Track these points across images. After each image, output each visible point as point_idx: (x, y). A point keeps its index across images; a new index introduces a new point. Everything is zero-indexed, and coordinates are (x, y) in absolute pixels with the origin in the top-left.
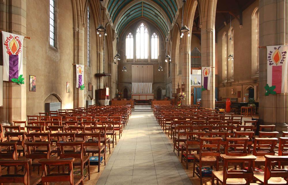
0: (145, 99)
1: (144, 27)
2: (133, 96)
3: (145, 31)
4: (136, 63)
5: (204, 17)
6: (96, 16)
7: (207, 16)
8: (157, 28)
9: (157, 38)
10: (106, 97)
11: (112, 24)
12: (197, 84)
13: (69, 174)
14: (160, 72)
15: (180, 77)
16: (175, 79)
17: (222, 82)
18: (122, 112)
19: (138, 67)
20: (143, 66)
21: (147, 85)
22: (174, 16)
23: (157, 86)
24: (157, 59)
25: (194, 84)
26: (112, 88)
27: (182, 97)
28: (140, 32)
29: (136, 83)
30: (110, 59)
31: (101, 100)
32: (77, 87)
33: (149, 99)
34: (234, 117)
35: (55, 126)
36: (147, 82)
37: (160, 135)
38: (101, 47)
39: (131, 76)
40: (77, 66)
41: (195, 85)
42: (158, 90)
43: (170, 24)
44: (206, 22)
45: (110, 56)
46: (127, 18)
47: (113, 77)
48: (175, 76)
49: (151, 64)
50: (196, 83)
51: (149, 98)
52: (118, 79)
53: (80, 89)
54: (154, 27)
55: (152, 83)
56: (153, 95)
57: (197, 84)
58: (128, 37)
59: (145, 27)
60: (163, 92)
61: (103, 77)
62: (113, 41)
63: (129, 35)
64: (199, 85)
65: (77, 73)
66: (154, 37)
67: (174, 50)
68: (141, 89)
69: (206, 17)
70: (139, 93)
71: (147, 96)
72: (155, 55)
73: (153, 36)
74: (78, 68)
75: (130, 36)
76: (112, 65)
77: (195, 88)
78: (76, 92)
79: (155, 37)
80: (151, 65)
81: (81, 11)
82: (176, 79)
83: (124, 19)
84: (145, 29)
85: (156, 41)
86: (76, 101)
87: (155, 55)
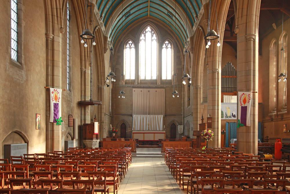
0: (152, 139)
1: (152, 32)
3: (153, 38)
4: (139, 85)
5: (242, 17)
9: (171, 48)
10: (94, 136)
12: (230, 117)
15: (204, 106)
16: (197, 109)
17: (269, 114)
19: (141, 91)
20: (149, 89)
22: (197, 16)
23: (170, 119)
24: (171, 80)
25: (227, 117)
27: (207, 137)
28: (145, 40)
29: (139, 116)
30: (100, 80)
31: (87, 141)
32: (52, 120)
38: (87, 62)
39: (132, 105)
40: (52, 90)
41: (227, 119)
48: (197, 105)
50: (229, 115)
51: (158, 137)
54: (165, 33)
55: (162, 116)
57: (230, 117)
58: (127, 46)
59: (153, 32)
60: (180, 129)
61: (90, 106)
62: (105, 53)
63: (129, 44)
64: (233, 118)
65: (51, 101)
66: (167, 48)
70: (144, 131)
71: (145, 134)
72: (168, 74)
73: (164, 46)
74: (53, 93)
75: (130, 46)
77: (228, 122)
78: (50, 129)
79: (168, 47)
80: (162, 89)
84: (152, 36)
86: (50, 141)
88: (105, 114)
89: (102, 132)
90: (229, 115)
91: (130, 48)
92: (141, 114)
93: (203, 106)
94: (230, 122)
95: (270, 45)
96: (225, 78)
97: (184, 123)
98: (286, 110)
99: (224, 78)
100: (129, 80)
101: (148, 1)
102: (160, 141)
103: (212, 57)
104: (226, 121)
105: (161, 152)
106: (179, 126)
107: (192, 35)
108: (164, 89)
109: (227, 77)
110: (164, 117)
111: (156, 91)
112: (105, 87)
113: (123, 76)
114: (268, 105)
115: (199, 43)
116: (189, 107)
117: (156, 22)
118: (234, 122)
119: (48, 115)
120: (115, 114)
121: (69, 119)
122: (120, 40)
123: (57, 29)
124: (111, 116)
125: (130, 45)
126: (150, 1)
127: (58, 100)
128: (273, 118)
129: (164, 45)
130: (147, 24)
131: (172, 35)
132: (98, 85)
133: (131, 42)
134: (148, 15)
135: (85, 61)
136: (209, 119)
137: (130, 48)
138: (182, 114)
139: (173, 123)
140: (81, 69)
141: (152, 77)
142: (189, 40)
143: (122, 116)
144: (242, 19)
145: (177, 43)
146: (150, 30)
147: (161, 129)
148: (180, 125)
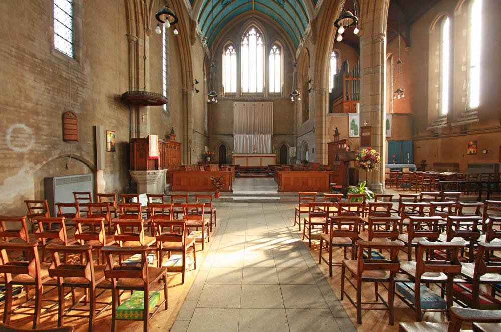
0: (258, 165)
1: (256, 34)
2: (236, 159)
3: (258, 42)
4: (242, 98)
5: (367, 13)
7: (374, 11)
8: (282, 34)
9: (280, 54)
10: (149, 163)
13: (182, 235)
14: (283, 115)
15: (332, 118)
16: (321, 122)
17: (427, 129)
22: (302, 37)
23: (280, 139)
24: (280, 93)
26: (191, 142)
27: (369, 163)
28: (248, 45)
29: (242, 136)
31: (135, 172)
33: (266, 165)
34: (464, 208)
36: (262, 134)
37: (276, 207)
39: (233, 123)
42: (282, 147)
43: (313, 7)
44: (371, 22)
45: (185, 74)
46: (224, 8)
47: (193, 119)
48: (321, 116)
49: (268, 101)
51: (266, 162)
52: (208, 127)
54: (275, 34)
55: (270, 136)
56: (274, 157)
58: (227, 53)
59: (258, 35)
60: (292, 151)
61: (149, 107)
62: (192, 44)
63: (230, 49)
66: (274, 54)
67: (320, 61)
68: (250, 147)
69: (370, 16)
70: (248, 154)
71: (263, 159)
72: (276, 86)
73: (271, 51)
75: (231, 52)
76: (191, 95)
79: (276, 53)
80: (270, 103)
82: (324, 123)
83: (215, 12)
84: (257, 39)
85: (277, 60)
87: (276, 86)
88: (194, 131)
89: (189, 156)
91: (231, 54)
92: (244, 134)
93: (330, 118)
97: (296, 144)
98: (477, 117)
100: (229, 93)
101: (251, 1)
102: (271, 168)
103: (372, 12)
105: (278, 191)
106: (290, 148)
107: (315, 18)
108: (272, 103)
110: (272, 138)
111: (244, 105)
112: (194, 94)
113: (222, 89)
114: (427, 116)
115: (327, 22)
116: (306, 122)
117: (264, 20)
120: (213, 134)
121: (63, 124)
122: (218, 41)
124: (207, 135)
125: (231, 50)
126: (254, 1)
128: (438, 134)
129: (272, 50)
130: (251, 21)
131: (282, 34)
132: (183, 90)
133: (232, 48)
134: (252, 9)
135: (136, 22)
136: (363, 130)
137: (231, 54)
138: (294, 133)
139: (284, 145)
140: (128, 35)
142: (308, 28)
143: (221, 136)
144: (367, 16)
145: (287, 42)
146: (255, 33)
147: (269, 151)
148: (291, 146)
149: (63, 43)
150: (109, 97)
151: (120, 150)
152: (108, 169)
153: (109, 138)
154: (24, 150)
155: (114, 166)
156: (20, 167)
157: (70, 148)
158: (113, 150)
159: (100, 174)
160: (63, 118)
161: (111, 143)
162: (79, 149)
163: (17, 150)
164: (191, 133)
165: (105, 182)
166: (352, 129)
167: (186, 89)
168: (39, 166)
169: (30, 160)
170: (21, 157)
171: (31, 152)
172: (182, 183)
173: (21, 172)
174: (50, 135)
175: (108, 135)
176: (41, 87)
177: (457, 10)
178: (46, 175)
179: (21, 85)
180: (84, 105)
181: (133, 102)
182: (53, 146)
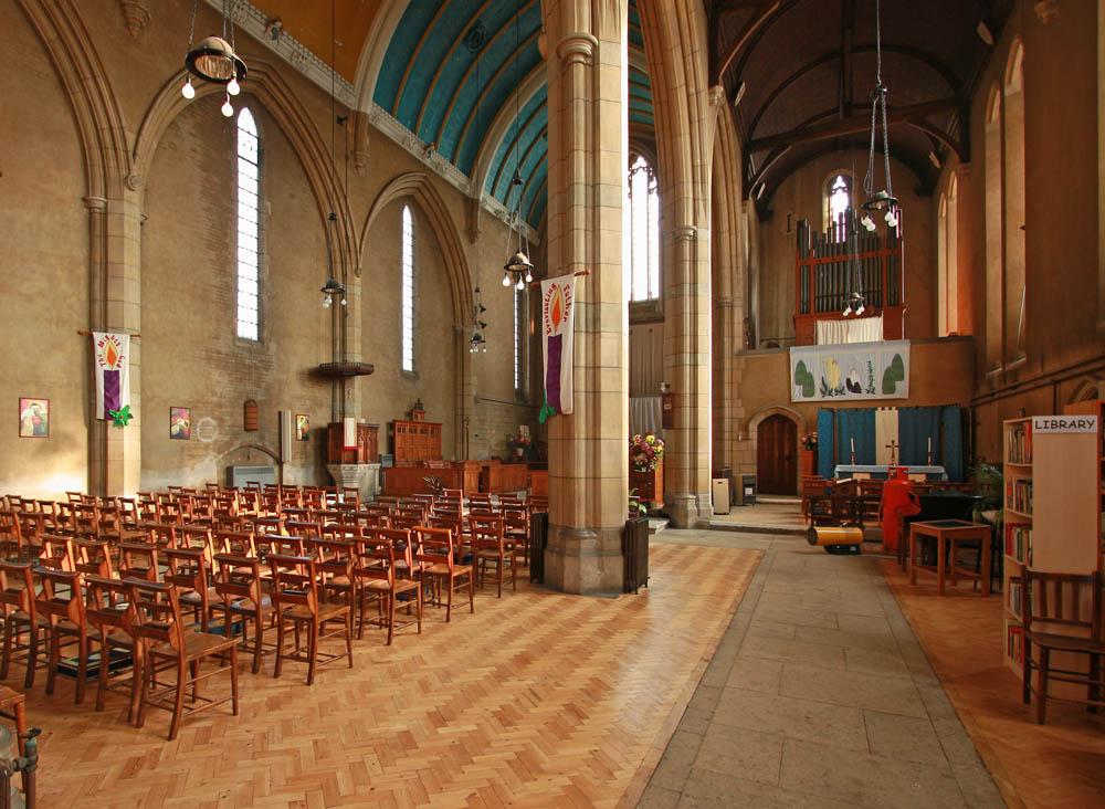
6: (308, 150)
10: (345, 456)
11: (454, 176)
15: (747, 360)
18: (195, 517)
21: (649, 404)
25: (826, 390)
30: (459, 314)
31: (329, 466)
32: (100, 414)
35: (444, 530)
38: (349, 266)
40: (98, 336)
41: (828, 398)
47: (474, 379)
50: (834, 384)
53: (110, 423)
64: (850, 396)
65: (98, 364)
72: (656, 295)
74: (101, 344)
77: (832, 410)
78: (98, 436)
81: (111, 129)
86: (98, 465)
90: (834, 384)
94: (839, 410)
95: (985, 114)
96: (833, 264)
99: (828, 264)
104: (819, 405)
109: (838, 259)
111: (651, 331)
118: (857, 410)
119: (93, 402)
121: (245, 413)
123: (117, 179)
127: (117, 362)
141: (649, 293)
149: (247, 327)
150: (302, 374)
151: (315, 439)
152: (298, 462)
153: (298, 424)
154: (209, 441)
155: (306, 458)
156: (205, 456)
157: (251, 438)
158: (305, 438)
159: (286, 468)
160: (245, 407)
161: (303, 430)
162: (262, 438)
163: (204, 440)
164: (469, 403)
165: (295, 474)
166: (798, 383)
167: (460, 324)
168: (221, 456)
169: (214, 450)
170: (207, 447)
171: (216, 442)
172: (396, 484)
173: (207, 460)
174: (233, 425)
175: (299, 421)
176: (225, 380)
177: (1010, 82)
178: (228, 465)
179: (209, 382)
180: (268, 389)
181: (333, 375)
182: (235, 436)
